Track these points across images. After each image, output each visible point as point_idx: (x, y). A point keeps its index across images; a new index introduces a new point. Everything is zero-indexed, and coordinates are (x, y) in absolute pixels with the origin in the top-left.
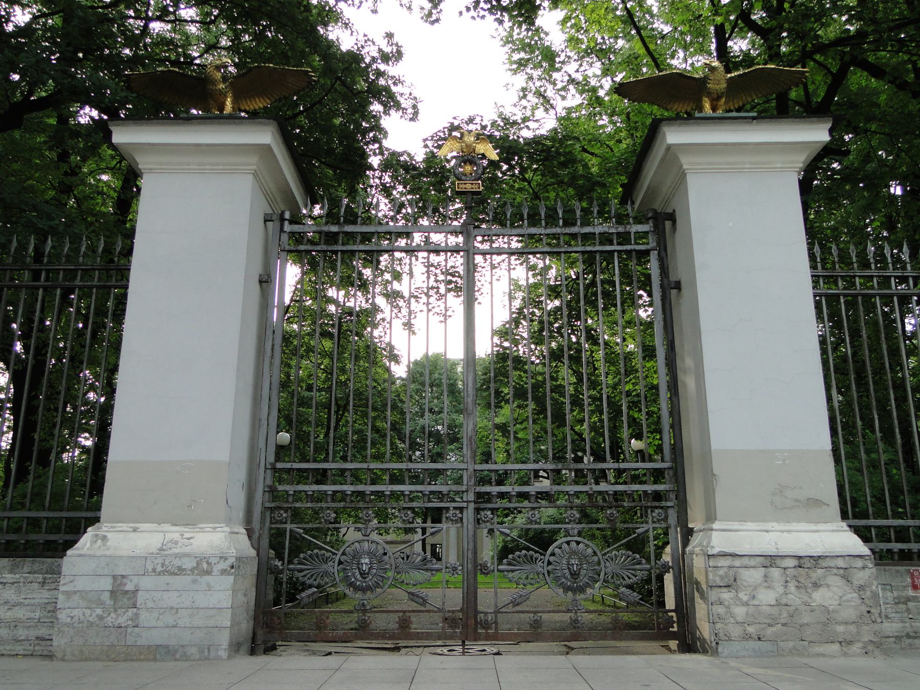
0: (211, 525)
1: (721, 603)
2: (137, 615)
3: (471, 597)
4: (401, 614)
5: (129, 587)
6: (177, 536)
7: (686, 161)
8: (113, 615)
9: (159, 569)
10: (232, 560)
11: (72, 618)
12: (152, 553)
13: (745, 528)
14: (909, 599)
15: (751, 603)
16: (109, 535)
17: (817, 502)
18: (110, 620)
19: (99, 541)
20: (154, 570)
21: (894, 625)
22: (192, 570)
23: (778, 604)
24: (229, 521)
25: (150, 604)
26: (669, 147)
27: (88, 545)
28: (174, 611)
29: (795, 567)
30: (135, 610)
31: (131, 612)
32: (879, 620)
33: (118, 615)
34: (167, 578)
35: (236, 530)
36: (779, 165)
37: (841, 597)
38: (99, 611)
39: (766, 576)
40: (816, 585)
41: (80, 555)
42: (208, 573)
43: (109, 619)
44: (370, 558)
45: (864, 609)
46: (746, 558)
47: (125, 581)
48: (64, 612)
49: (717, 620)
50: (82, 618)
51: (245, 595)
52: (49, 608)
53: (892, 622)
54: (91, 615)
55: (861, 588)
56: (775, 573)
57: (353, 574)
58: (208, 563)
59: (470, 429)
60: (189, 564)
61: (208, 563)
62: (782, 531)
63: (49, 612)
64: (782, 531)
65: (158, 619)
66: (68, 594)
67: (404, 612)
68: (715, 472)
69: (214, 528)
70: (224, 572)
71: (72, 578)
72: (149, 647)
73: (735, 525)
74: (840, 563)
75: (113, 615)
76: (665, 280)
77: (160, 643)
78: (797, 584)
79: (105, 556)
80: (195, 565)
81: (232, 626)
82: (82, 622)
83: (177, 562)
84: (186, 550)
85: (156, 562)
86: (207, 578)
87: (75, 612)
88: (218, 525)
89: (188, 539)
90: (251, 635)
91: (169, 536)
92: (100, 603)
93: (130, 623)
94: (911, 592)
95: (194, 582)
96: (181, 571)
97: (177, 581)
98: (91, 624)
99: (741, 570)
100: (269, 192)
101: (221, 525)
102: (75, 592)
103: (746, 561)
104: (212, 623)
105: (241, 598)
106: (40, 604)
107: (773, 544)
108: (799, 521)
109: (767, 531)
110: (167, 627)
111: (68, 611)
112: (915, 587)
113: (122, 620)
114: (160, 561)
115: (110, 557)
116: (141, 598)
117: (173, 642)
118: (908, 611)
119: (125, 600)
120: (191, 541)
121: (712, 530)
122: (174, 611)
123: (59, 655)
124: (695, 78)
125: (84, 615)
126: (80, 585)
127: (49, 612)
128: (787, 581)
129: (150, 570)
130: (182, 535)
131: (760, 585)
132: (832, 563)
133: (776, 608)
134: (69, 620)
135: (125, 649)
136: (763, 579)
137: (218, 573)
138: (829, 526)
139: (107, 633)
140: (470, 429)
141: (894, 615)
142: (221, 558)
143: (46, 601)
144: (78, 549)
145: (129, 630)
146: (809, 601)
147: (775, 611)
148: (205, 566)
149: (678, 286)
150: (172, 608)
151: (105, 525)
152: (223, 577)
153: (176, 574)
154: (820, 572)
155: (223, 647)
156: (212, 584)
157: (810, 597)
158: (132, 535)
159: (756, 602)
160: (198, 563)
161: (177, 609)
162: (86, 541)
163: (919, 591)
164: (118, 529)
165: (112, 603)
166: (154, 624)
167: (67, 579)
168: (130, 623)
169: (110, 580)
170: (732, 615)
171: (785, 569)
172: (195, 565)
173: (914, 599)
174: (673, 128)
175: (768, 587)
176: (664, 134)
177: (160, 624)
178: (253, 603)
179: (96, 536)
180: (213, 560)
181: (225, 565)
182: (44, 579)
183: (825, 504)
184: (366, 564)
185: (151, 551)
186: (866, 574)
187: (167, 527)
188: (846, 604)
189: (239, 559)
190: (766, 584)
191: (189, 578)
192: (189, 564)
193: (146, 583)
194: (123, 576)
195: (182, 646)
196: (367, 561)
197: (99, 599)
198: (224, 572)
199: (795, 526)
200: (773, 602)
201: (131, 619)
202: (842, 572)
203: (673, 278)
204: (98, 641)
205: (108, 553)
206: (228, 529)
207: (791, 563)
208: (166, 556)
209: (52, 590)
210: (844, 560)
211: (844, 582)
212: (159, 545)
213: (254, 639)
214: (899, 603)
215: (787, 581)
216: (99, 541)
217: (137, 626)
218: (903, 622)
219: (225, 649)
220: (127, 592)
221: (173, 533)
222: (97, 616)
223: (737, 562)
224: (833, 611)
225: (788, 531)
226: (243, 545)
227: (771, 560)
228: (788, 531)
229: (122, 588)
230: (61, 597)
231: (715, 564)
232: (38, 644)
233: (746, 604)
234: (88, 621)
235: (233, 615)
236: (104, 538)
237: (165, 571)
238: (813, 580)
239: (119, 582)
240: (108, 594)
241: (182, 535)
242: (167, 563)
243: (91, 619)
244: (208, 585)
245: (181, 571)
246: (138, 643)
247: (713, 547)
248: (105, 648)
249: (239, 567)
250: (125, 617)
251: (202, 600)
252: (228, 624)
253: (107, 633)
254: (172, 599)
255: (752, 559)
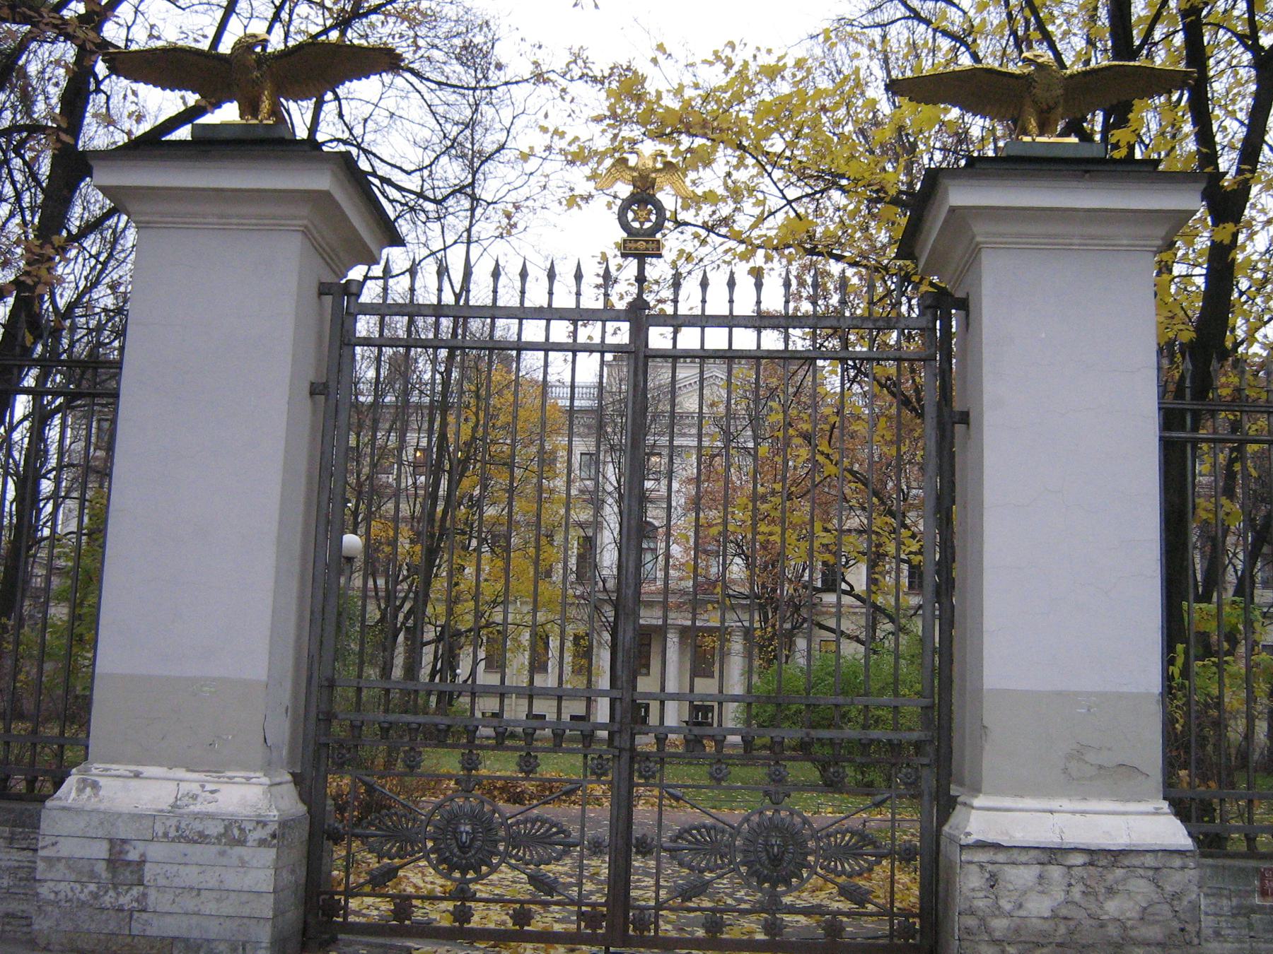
0: (243, 774)
1: (972, 914)
2: (145, 895)
3: (620, 881)
4: (518, 906)
5: (133, 856)
6: (195, 788)
7: (981, 231)
8: (111, 893)
9: (172, 833)
10: (273, 827)
11: (56, 893)
12: (162, 811)
13: (1021, 806)
14: (1254, 910)
15: (1016, 913)
16: (102, 781)
17: (1131, 770)
18: (108, 899)
19: (88, 789)
20: (166, 835)
21: (1228, 945)
22: (219, 838)
23: (1055, 916)
24: (268, 768)
25: (162, 881)
26: (953, 210)
27: (73, 794)
28: (194, 893)
29: (1084, 865)
30: (141, 888)
31: (136, 891)
32: (1196, 941)
33: (118, 894)
34: (183, 847)
35: (278, 780)
36: (1125, 242)
37: (1145, 909)
38: (93, 887)
39: (1040, 877)
40: (1111, 891)
41: (64, 808)
42: (242, 842)
43: (107, 898)
44: (473, 825)
45: (1176, 925)
46: (1015, 851)
47: (127, 847)
48: (46, 884)
49: (965, 936)
50: (70, 894)
51: (293, 872)
52: (22, 874)
53: (1226, 941)
54: (82, 892)
55: (1176, 896)
56: (1055, 872)
57: (448, 846)
58: (241, 829)
59: (628, 638)
60: (214, 829)
61: (241, 829)
62: (1074, 813)
63: (21, 879)
64: (1074, 813)
65: (174, 902)
66: (48, 860)
67: (522, 902)
68: (985, 723)
69: (248, 779)
70: (262, 843)
71: (54, 839)
72: (163, 938)
73: (1007, 802)
74: (1150, 860)
75: (111, 893)
76: (946, 410)
77: (177, 934)
78: (1083, 888)
79: (97, 811)
80: (222, 831)
81: (275, 916)
82: (71, 900)
83: (198, 826)
84: (211, 808)
85: (168, 823)
86: (238, 850)
87: (62, 886)
88: (252, 775)
89: (212, 792)
90: (301, 926)
91: (185, 787)
92: (93, 875)
93: (135, 904)
94: (1257, 901)
95: (222, 854)
96: (202, 838)
97: (196, 851)
98: (83, 904)
99: (1006, 868)
100: (327, 248)
101: (258, 774)
102: (59, 859)
103: (1015, 855)
104: (246, 911)
105: (286, 876)
106: (8, 868)
107: (1057, 831)
108: (1100, 796)
109: (1051, 812)
110: (186, 914)
111: (51, 884)
112: (1264, 893)
113: (125, 900)
114: (174, 822)
115: (104, 813)
116: (149, 871)
117: (195, 934)
118: (1250, 926)
119: (127, 873)
120: (215, 795)
121: (973, 808)
122: (194, 893)
123: (42, 943)
124: (1012, 75)
125: (72, 889)
126: (67, 848)
127: (21, 879)
128: (1070, 885)
129: (160, 834)
130: (203, 786)
131: (1031, 889)
132: (1136, 861)
133: (1051, 923)
134: (52, 896)
135: (129, 940)
136: (1036, 880)
137: (255, 844)
138: (1148, 806)
139: (104, 917)
140: (628, 638)
141: (1229, 931)
142: (258, 822)
143: (16, 864)
144: (60, 799)
145: (136, 915)
146: (1099, 912)
147: (1046, 926)
148: (236, 832)
149: (965, 418)
150: (192, 889)
151: (96, 765)
152: (261, 849)
153: (195, 842)
154: (1119, 873)
155: (264, 945)
156: (246, 859)
157: (1101, 908)
158: (134, 783)
159: (1022, 913)
160: (226, 828)
161: (199, 890)
162: (70, 790)
163: (1270, 899)
164: (113, 772)
165: (110, 876)
166: (167, 908)
167: (48, 840)
168: (135, 904)
169: (105, 846)
170: (988, 931)
171: (1070, 867)
172: (222, 831)
173: (1261, 909)
174: (957, 182)
175: (1043, 892)
176: (946, 192)
177: (175, 908)
178: (303, 881)
179: (84, 780)
180: (249, 826)
181: (261, 833)
182: (12, 833)
183: (1143, 773)
184: (467, 833)
185: (160, 807)
186: (1184, 878)
187: (181, 773)
188: (1152, 918)
189: (283, 824)
190: (1040, 888)
191: (214, 849)
192: (214, 829)
193: (156, 851)
194: (124, 841)
195: (208, 940)
196: (468, 828)
197: (92, 871)
198: (262, 843)
199: (1093, 805)
200: (1047, 914)
201: (137, 900)
202: (1150, 873)
203: (957, 406)
204: (93, 927)
205: (102, 807)
206: (265, 780)
207: (1079, 859)
208: (182, 816)
209: (24, 849)
210: (1156, 858)
211: (1153, 887)
212: (172, 800)
213: (304, 931)
214: (1239, 914)
215: (1070, 885)
216: (88, 789)
217: (144, 910)
218: (1241, 942)
219: (266, 948)
220: (129, 863)
221: (191, 782)
222: (91, 892)
223: (1001, 857)
224: (1132, 928)
225: (1083, 813)
226: (289, 803)
227: (1052, 854)
228: (1083, 813)
229: (123, 857)
230: (41, 865)
231: (969, 858)
232: (8, 924)
233: (1010, 915)
234: (78, 899)
235: (276, 902)
236: (95, 786)
237: (181, 836)
238: (1108, 884)
239: (118, 848)
240: (103, 865)
241: (203, 786)
242: (183, 825)
243: (82, 897)
244: (241, 858)
245: (202, 838)
246: (148, 933)
247: (969, 834)
248: (102, 937)
249: (283, 834)
250: (128, 898)
251: (233, 880)
252: (271, 915)
253: (104, 917)
254: (190, 875)
255: (1024, 853)
